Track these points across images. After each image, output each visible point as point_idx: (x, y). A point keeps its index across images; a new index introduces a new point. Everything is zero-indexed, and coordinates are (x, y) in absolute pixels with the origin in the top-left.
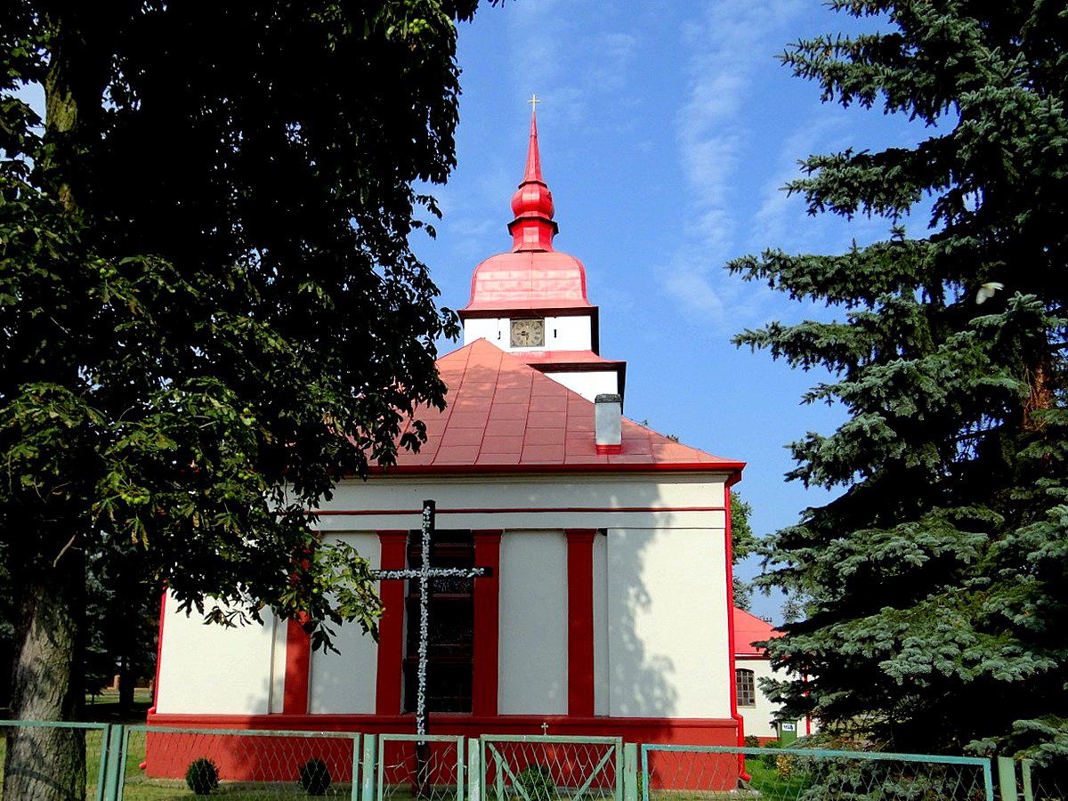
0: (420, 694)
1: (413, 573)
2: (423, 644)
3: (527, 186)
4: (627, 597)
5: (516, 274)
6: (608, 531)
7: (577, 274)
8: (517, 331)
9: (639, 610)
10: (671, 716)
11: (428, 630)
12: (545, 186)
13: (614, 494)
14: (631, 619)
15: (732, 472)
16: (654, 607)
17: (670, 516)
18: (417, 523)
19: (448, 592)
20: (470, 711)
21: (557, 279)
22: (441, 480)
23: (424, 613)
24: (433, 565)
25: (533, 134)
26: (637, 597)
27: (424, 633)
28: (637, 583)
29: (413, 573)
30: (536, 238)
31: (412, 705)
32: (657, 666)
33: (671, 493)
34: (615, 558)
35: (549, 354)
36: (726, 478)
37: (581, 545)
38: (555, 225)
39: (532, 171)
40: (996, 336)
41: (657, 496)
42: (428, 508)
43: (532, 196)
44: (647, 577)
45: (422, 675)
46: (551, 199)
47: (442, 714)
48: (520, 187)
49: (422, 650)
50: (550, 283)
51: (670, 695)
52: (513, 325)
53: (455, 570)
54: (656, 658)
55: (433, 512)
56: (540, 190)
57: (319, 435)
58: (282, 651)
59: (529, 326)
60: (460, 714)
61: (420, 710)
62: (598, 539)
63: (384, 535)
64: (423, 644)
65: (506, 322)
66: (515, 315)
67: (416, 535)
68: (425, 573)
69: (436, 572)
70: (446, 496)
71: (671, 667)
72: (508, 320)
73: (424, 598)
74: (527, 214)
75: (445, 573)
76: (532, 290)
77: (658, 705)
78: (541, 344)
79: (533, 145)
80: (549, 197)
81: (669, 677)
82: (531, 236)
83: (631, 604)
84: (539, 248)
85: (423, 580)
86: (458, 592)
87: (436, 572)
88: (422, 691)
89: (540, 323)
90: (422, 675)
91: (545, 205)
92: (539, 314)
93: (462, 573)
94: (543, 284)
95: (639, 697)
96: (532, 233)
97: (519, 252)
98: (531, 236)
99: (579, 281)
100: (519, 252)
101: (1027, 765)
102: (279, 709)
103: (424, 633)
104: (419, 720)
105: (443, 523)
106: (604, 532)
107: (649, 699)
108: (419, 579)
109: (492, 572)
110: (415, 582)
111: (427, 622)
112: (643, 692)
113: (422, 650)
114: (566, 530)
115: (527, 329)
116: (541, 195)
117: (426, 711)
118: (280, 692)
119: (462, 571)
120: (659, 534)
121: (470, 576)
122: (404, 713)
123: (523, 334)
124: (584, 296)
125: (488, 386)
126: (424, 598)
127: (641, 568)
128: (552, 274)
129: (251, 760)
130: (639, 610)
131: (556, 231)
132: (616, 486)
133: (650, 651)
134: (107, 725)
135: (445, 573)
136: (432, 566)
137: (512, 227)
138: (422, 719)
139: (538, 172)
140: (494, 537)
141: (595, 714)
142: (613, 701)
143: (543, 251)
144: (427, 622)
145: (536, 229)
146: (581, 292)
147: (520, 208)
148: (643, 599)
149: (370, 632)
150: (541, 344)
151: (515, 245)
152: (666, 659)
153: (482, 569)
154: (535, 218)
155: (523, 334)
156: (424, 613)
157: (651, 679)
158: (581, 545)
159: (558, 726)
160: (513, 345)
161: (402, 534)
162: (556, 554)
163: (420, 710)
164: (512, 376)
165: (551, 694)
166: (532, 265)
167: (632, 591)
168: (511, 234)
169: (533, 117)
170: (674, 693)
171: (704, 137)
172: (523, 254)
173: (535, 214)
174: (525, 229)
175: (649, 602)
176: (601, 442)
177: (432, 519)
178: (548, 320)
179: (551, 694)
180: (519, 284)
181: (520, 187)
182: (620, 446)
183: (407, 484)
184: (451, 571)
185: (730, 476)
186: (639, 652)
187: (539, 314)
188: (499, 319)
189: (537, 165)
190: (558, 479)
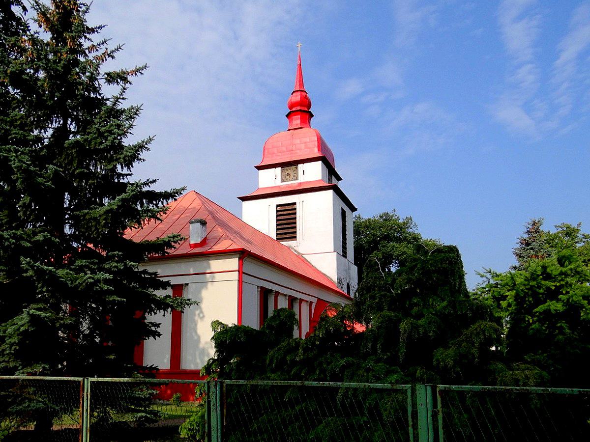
8: (285, 174)
9: (199, 320)
13: (191, 267)
14: (196, 325)
17: (214, 277)
22: (157, 263)
25: (299, 64)
26: (199, 315)
30: (298, 122)
32: (206, 346)
33: (216, 264)
35: (300, 184)
40: (15, 224)
41: (209, 267)
52: (282, 171)
59: (290, 170)
65: (279, 169)
66: (283, 165)
72: (280, 168)
74: (294, 109)
78: (297, 179)
82: (297, 121)
83: (196, 318)
84: (300, 127)
89: (297, 168)
92: (295, 163)
96: (297, 119)
98: (297, 121)
101: (89, 380)
106: (187, 284)
115: (289, 172)
123: (288, 174)
130: (199, 320)
134: (82, 378)
137: (288, 116)
145: (299, 116)
148: (201, 315)
150: (297, 179)
154: (298, 111)
155: (288, 174)
159: (166, 374)
160: (283, 181)
165: (166, 361)
167: (197, 312)
169: (299, 54)
171: (519, 18)
172: (291, 131)
173: (299, 108)
174: (294, 117)
175: (204, 316)
176: (192, 242)
178: (300, 166)
183: (187, 262)
187: (295, 163)
188: (303, 164)
190: (169, 262)
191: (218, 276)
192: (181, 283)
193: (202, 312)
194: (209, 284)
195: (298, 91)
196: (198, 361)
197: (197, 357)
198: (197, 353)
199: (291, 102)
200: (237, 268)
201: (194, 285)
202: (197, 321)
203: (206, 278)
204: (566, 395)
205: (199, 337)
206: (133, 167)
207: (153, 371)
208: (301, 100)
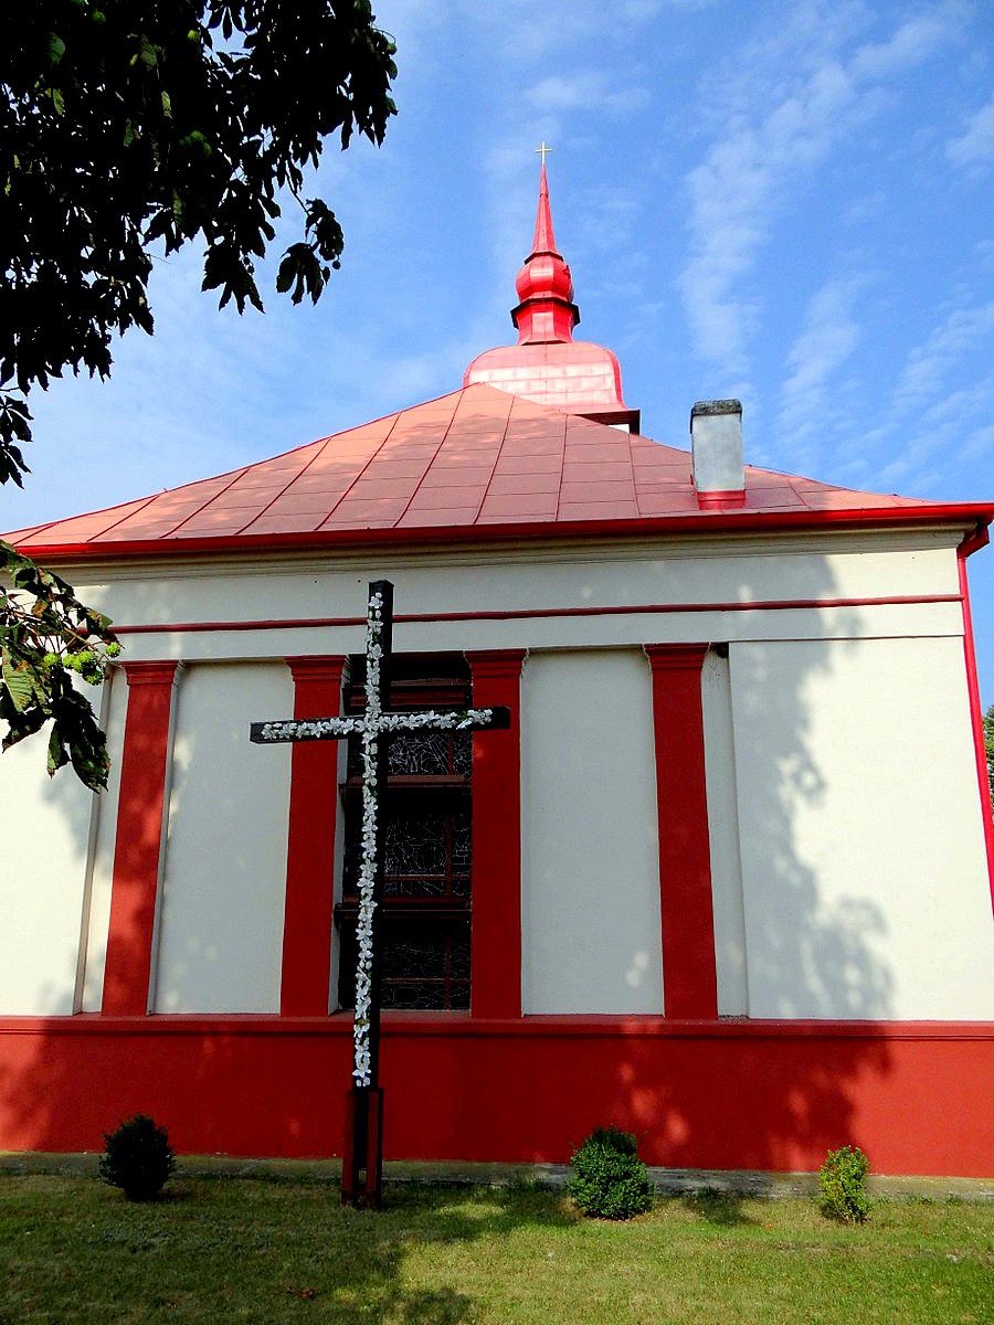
0: (361, 975)
1: (348, 725)
2: (368, 870)
3: (535, 259)
4: (778, 778)
5: (523, 373)
6: (725, 660)
7: (608, 369)
9: (800, 804)
10: (877, 1015)
11: (377, 839)
12: (561, 258)
14: (786, 822)
15: (971, 526)
16: (830, 796)
18: (356, 642)
19: (420, 772)
20: (465, 1005)
21: (580, 377)
23: (371, 806)
24: (387, 707)
26: (797, 778)
27: (370, 846)
28: (796, 748)
29: (348, 725)
30: (550, 326)
31: (348, 1000)
32: (849, 920)
33: (857, 570)
34: (749, 701)
36: (960, 538)
37: (677, 675)
38: (575, 310)
39: (543, 240)
41: (828, 580)
42: (379, 595)
43: (542, 271)
44: (822, 741)
45: (364, 934)
46: (569, 276)
47: (412, 1015)
48: (526, 262)
49: (366, 883)
50: (570, 384)
51: (879, 982)
53: (432, 715)
54: (847, 904)
55: (388, 617)
56: (555, 264)
57: (27, 229)
58: (104, 889)
60: (447, 1015)
61: (361, 1009)
62: (711, 664)
63: (299, 665)
64: (368, 870)
67: (358, 662)
68: (372, 723)
69: (394, 721)
70: (417, 589)
71: (879, 923)
73: (370, 775)
74: (537, 296)
75: (412, 722)
76: (546, 392)
77: (854, 999)
79: (543, 205)
80: (566, 272)
81: (876, 945)
82: (543, 322)
83: (786, 791)
85: (368, 737)
86: (438, 772)
87: (394, 721)
88: (364, 969)
90: (364, 934)
91: (561, 283)
93: (445, 721)
94: (560, 385)
95: (814, 984)
97: (527, 344)
98: (543, 322)
99: (612, 378)
100: (527, 344)
102: (93, 1001)
103: (370, 846)
104: (359, 1031)
105: (407, 640)
106: (722, 650)
107: (837, 987)
108: (359, 736)
109: (507, 719)
110: (355, 738)
111: (376, 823)
112: (822, 974)
113: (366, 883)
114: (647, 646)
116: (555, 270)
117: (373, 1013)
118: (97, 972)
119: (448, 717)
120: (837, 652)
121: (463, 725)
122: (337, 1012)
124: (619, 398)
125: (495, 438)
126: (370, 775)
127: (805, 723)
128: (572, 371)
129: (43, 1117)
130: (800, 804)
131: (577, 320)
132: (752, 562)
133: (831, 891)
135: (412, 722)
136: (387, 707)
137: (515, 313)
138: (366, 1028)
139: (550, 242)
140: (508, 664)
141: (721, 1012)
142: (761, 984)
143: (560, 342)
144: (376, 823)
146: (614, 393)
147: (527, 289)
148: (809, 779)
149: (70, 763)
151: (521, 338)
152: (867, 906)
153: (489, 712)
156: (371, 806)
157: (837, 949)
158: (677, 675)
161: (334, 662)
162: (628, 697)
163: (361, 1009)
164: (534, 424)
165: (633, 978)
166: (546, 361)
167: (788, 766)
168: (516, 326)
170: (887, 977)
173: (549, 294)
174: (535, 315)
175: (821, 785)
177: (387, 631)
179: (633, 978)
180: (529, 386)
181: (526, 262)
182: (743, 492)
184: (425, 718)
185: (968, 534)
186: (806, 889)
189: (549, 232)
191: (875, 619)
192: (706, 641)
193: (809, 766)
194: (837, 649)
195: (546, 254)
196: (814, 984)
197: (809, 966)
198: (806, 949)
199: (526, 279)
200: (395, 626)
201: (758, 652)
202: (792, 808)
203: (819, 622)
204: (105, 767)
205: (809, 879)
206: (30, 418)
207: (592, 1040)
208: (555, 275)
